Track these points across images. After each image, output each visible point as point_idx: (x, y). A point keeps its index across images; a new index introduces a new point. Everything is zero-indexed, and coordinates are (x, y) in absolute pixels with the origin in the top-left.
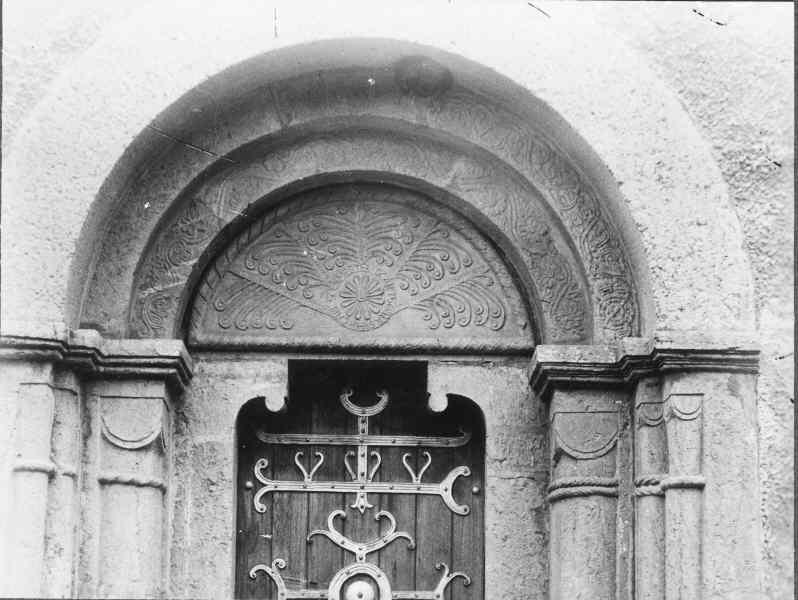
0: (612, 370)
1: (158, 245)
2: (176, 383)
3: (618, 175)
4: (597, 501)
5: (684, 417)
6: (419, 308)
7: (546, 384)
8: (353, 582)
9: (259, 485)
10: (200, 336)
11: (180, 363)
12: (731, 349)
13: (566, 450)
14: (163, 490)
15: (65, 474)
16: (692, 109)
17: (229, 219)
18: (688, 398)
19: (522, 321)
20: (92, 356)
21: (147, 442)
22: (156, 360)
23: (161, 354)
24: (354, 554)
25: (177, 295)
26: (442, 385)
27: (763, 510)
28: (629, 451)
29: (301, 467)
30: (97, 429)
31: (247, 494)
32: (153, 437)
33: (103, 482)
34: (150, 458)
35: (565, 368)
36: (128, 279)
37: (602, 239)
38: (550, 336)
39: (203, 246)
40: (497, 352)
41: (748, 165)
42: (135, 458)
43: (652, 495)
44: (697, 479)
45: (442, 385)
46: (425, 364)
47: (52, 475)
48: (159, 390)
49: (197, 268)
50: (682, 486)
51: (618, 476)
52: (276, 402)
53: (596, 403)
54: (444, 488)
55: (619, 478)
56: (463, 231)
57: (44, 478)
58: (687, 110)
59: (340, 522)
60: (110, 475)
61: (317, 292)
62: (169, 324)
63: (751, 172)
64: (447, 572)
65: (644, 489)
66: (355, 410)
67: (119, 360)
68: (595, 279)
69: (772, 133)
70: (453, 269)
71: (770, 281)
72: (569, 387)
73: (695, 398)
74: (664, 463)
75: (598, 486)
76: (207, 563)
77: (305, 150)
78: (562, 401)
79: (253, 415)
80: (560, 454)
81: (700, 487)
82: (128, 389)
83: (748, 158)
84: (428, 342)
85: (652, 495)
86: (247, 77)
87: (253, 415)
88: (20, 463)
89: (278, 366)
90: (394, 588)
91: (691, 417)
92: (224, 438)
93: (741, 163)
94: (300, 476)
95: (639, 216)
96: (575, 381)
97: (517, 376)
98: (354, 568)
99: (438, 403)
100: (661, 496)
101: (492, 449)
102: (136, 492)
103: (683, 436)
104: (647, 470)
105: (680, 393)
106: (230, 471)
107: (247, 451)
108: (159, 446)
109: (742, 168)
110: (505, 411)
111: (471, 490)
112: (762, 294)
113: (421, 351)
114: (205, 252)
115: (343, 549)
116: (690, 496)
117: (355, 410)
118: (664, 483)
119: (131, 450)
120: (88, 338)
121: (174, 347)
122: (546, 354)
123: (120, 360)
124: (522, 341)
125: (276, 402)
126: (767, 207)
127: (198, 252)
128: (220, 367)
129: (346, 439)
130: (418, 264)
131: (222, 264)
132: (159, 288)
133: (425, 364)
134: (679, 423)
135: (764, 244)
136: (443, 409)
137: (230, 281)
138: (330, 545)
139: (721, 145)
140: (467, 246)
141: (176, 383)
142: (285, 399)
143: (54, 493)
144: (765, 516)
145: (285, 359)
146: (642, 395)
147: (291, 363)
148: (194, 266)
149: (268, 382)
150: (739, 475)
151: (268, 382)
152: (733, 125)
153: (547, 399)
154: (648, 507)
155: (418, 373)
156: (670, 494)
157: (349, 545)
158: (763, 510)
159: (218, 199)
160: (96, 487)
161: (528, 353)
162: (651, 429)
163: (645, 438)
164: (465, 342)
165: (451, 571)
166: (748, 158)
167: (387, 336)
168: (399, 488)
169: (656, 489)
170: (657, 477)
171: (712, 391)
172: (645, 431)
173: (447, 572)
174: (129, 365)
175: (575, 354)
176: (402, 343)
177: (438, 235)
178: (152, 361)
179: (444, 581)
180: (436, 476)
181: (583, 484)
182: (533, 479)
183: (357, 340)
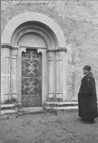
0: (55, 50)
3: (56, 34)
6: (37, 44)
8: (32, 36)
9: (28, 81)
26: (39, 51)
30: (11, 53)
33: (12, 58)
34: (16, 57)
36: (14, 40)
40: (44, 48)
44: (62, 60)
45: (39, 51)
46: (37, 49)
50: (61, 60)
52: (25, 52)
54: (38, 59)
57: (8, 58)
60: (13, 58)
61: (28, 42)
66: (31, 52)
74: (59, 58)
79: (23, 53)
81: (62, 60)
82: (14, 50)
84: (38, 47)
88: (7, 57)
89: (25, 48)
90: (34, 67)
94: (26, 58)
95: (57, 38)
98: (31, 66)
99: (39, 52)
100: (59, 61)
103: (61, 56)
107: (22, 55)
111: (41, 59)
113: (38, 48)
116: (61, 61)
117: (31, 52)
124: (46, 47)
125: (25, 52)
131: (20, 39)
137: (21, 40)
147: (26, 48)
154: (58, 62)
156: (60, 61)
168: (34, 59)
175: (51, 49)
180: (37, 58)
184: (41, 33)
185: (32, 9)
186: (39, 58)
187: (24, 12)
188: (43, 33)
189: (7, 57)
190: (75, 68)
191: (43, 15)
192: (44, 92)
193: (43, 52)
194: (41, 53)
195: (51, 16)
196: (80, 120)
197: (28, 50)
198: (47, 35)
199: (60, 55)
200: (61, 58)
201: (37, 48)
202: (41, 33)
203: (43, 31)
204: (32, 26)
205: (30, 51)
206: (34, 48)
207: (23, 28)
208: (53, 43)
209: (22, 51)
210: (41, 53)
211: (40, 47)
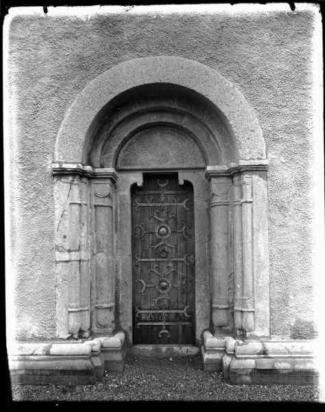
0: (228, 171)
2: (113, 179)
7: (209, 176)
14: (112, 208)
19: (202, 160)
33: (95, 206)
34: (107, 199)
36: (99, 152)
38: (210, 162)
39: (119, 143)
46: (177, 173)
47: (80, 205)
48: (109, 182)
51: (229, 200)
52: (140, 184)
53: (223, 180)
54: (183, 204)
60: (97, 204)
65: (237, 203)
72: (215, 177)
77: (143, 117)
78: (214, 180)
80: (213, 194)
81: (253, 312)
86: (176, 135)
87: (134, 188)
96: (217, 175)
99: (181, 182)
101: (196, 193)
104: (237, 198)
105: (246, 178)
108: (109, 196)
116: (249, 205)
117: (161, 185)
118: (242, 201)
120: (88, 168)
122: (209, 168)
125: (140, 183)
129: (159, 192)
145: (142, 172)
146: (236, 179)
147: (143, 173)
149: (138, 179)
151: (138, 179)
153: (209, 180)
154: (237, 208)
155: (176, 174)
161: (204, 168)
163: (236, 190)
167: (167, 165)
175: (218, 168)
176: (172, 167)
179: (184, 228)
183: (160, 167)
185: (145, 46)
187: (121, 61)
188: (245, 238)
189: (71, 204)
190: (303, 226)
192: (200, 301)
193: (195, 179)
197: (149, 177)
200: (249, 195)
204: (152, 105)
209: (194, 184)
210: (188, 186)
211: (185, 166)
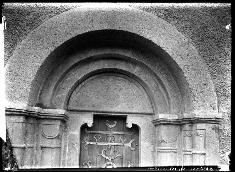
0: (178, 121)
1: (60, 84)
4: (172, 153)
5: (201, 135)
7: (157, 123)
10: (71, 107)
11: (65, 116)
12: (214, 118)
13: (164, 140)
15: (28, 147)
16: (202, 54)
17: (79, 78)
18: (201, 130)
20: (38, 114)
21: (54, 137)
22: (57, 115)
23: (59, 113)
24: (108, 160)
25: (65, 97)
27: (221, 161)
28: (180, 141)
29: (96, 139)
31: (82, 145)
32: (57, 135)
33: (42, 147)
35: (166, 120)
37: (173, 87)
41: (216, 70)
42: (51, 141)
43: (190, 155)
46: (127, 116)
49: (70, 90)
52: (90, 125)
55: (177, 148)
56: (137, 84)
58: (200, 54)
59: (105, 152)
60: (44, 145)
62: (62, 105)
63: (217, 71)
64: (130, 164)
66: (109, 126)
67: (45, 115)
68: (171, 98)
69: (221, 62)
70: (134, 93)
71: (221, 100)
73: (203, 130)
75: (173, 150)
76: (72, 164)
79: (84, 127)
82: (46, 122)
83: (216, 68)
85: (190, 155)
91: (202, 135)
92: (77, 133)
93: (214, 69)
97: (148, 119)
99: (130, 126)
102: (51, 150)
106: (78, 141)
108: (58, 137)
109: (214, 70)
110: (146, 128)
111: (136, 145)
112: (219, 103)
114: (73, 86)
115: (105, 159)
117: (109, 126)
119: (50, 139)
121: (61, 111)
123: (47, 115)
124: (150, 111)
126: (220, 81)
127: (70, 86)
128: (75, 115)
130: (126, 92)
132: (60, 95)
133: (127, 116)
134: (199, 137)
135: (220, 90)
136: (131, 127)
138: (100, 146)
139: (209, 64)
140: (138, 88)
141: (64, 121)
142: (93, 124)
143: (24, 153)
144: (222, 162)
145: (93, 114)
148: (70, 90)
150: (215, 151)
152: (212, 59)
157: (107, 158)
158: (221, 161)
159: (76, 73)
160: (40, 148)
162: (189, 137)
164: (137, 111)
165: (131, 164)
166: (216, 68)
169: (191, 153)
170: (191, 150)
171: (208, 129)
172: (187, 138)
173: (130, 164)
174: (53, 116)
177: (130, 85)
178: (56, 115)
181: (169, 149)
182: (152, 144)
184: (122, 66)
186: (131, 142)
191: (184, 69)
194: (135, 128)
195: (168, 14)
196: (212, 128)
198: (156, 75)
199: (197, 138)
201: (125, 115)
202: (122, 66)
203: (142, 65)
205: (85, 129)
206: (114, 113)
207: (84, 57)
208: (172, 100)
210: (135, 128)
